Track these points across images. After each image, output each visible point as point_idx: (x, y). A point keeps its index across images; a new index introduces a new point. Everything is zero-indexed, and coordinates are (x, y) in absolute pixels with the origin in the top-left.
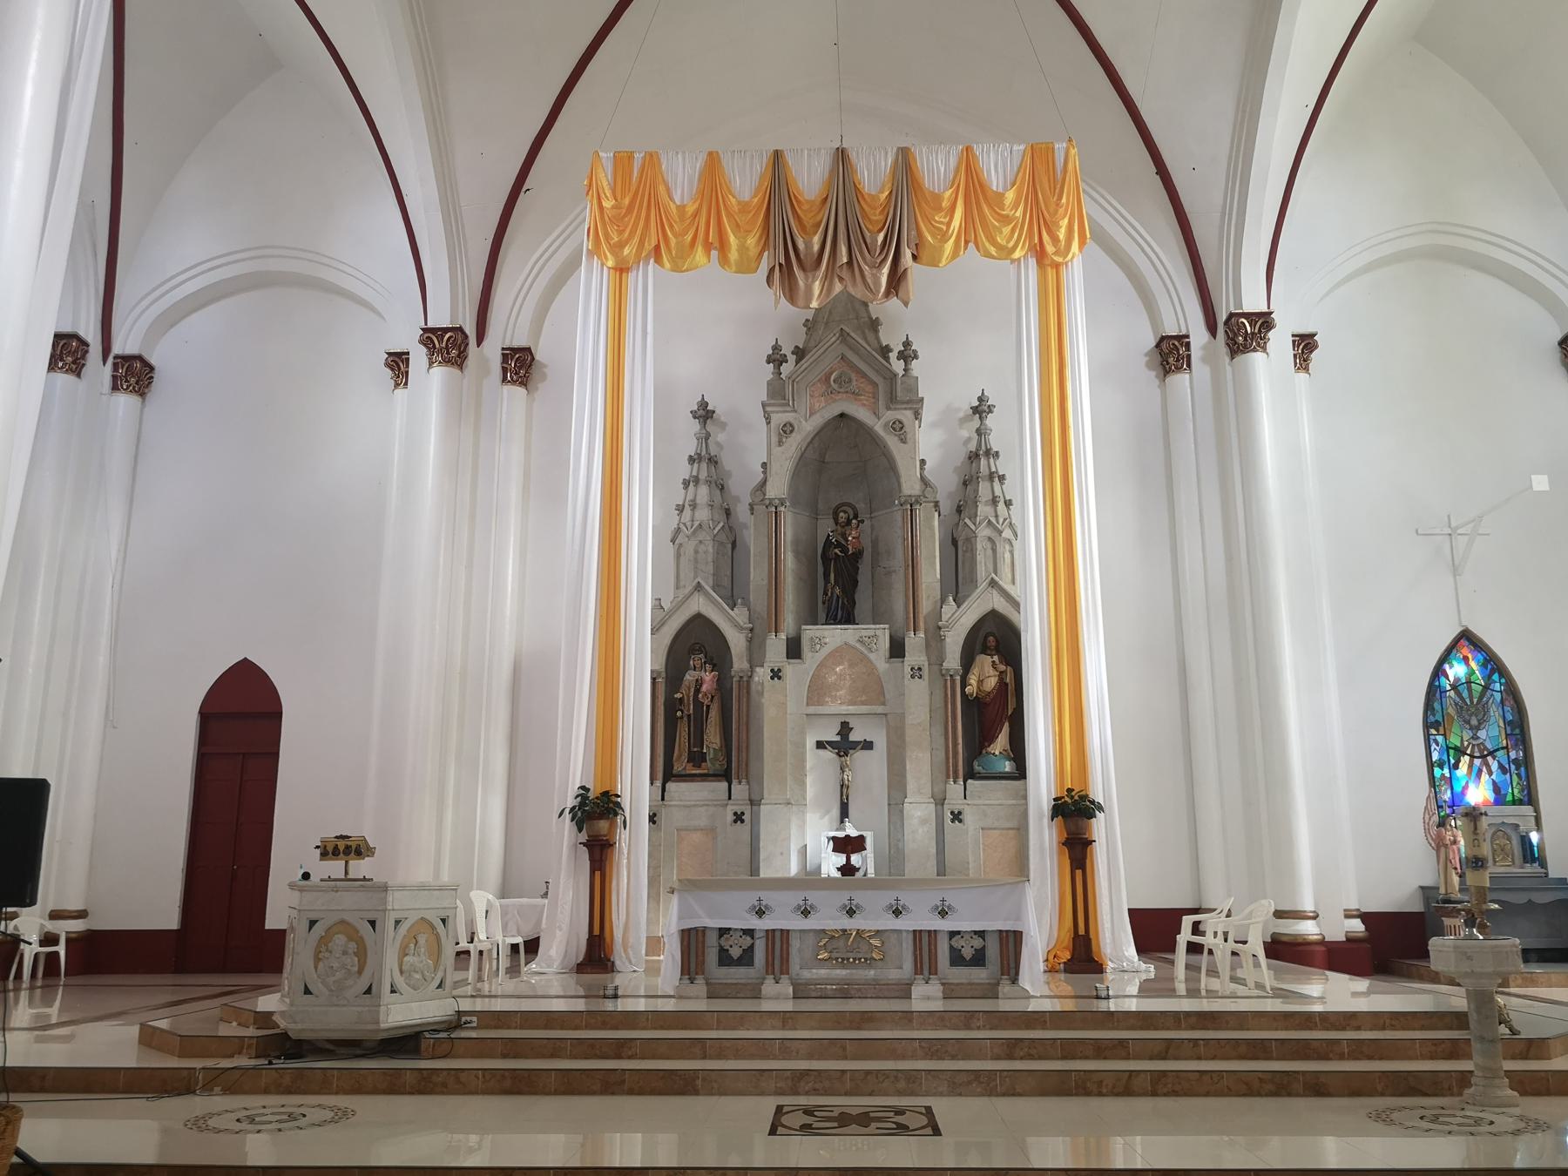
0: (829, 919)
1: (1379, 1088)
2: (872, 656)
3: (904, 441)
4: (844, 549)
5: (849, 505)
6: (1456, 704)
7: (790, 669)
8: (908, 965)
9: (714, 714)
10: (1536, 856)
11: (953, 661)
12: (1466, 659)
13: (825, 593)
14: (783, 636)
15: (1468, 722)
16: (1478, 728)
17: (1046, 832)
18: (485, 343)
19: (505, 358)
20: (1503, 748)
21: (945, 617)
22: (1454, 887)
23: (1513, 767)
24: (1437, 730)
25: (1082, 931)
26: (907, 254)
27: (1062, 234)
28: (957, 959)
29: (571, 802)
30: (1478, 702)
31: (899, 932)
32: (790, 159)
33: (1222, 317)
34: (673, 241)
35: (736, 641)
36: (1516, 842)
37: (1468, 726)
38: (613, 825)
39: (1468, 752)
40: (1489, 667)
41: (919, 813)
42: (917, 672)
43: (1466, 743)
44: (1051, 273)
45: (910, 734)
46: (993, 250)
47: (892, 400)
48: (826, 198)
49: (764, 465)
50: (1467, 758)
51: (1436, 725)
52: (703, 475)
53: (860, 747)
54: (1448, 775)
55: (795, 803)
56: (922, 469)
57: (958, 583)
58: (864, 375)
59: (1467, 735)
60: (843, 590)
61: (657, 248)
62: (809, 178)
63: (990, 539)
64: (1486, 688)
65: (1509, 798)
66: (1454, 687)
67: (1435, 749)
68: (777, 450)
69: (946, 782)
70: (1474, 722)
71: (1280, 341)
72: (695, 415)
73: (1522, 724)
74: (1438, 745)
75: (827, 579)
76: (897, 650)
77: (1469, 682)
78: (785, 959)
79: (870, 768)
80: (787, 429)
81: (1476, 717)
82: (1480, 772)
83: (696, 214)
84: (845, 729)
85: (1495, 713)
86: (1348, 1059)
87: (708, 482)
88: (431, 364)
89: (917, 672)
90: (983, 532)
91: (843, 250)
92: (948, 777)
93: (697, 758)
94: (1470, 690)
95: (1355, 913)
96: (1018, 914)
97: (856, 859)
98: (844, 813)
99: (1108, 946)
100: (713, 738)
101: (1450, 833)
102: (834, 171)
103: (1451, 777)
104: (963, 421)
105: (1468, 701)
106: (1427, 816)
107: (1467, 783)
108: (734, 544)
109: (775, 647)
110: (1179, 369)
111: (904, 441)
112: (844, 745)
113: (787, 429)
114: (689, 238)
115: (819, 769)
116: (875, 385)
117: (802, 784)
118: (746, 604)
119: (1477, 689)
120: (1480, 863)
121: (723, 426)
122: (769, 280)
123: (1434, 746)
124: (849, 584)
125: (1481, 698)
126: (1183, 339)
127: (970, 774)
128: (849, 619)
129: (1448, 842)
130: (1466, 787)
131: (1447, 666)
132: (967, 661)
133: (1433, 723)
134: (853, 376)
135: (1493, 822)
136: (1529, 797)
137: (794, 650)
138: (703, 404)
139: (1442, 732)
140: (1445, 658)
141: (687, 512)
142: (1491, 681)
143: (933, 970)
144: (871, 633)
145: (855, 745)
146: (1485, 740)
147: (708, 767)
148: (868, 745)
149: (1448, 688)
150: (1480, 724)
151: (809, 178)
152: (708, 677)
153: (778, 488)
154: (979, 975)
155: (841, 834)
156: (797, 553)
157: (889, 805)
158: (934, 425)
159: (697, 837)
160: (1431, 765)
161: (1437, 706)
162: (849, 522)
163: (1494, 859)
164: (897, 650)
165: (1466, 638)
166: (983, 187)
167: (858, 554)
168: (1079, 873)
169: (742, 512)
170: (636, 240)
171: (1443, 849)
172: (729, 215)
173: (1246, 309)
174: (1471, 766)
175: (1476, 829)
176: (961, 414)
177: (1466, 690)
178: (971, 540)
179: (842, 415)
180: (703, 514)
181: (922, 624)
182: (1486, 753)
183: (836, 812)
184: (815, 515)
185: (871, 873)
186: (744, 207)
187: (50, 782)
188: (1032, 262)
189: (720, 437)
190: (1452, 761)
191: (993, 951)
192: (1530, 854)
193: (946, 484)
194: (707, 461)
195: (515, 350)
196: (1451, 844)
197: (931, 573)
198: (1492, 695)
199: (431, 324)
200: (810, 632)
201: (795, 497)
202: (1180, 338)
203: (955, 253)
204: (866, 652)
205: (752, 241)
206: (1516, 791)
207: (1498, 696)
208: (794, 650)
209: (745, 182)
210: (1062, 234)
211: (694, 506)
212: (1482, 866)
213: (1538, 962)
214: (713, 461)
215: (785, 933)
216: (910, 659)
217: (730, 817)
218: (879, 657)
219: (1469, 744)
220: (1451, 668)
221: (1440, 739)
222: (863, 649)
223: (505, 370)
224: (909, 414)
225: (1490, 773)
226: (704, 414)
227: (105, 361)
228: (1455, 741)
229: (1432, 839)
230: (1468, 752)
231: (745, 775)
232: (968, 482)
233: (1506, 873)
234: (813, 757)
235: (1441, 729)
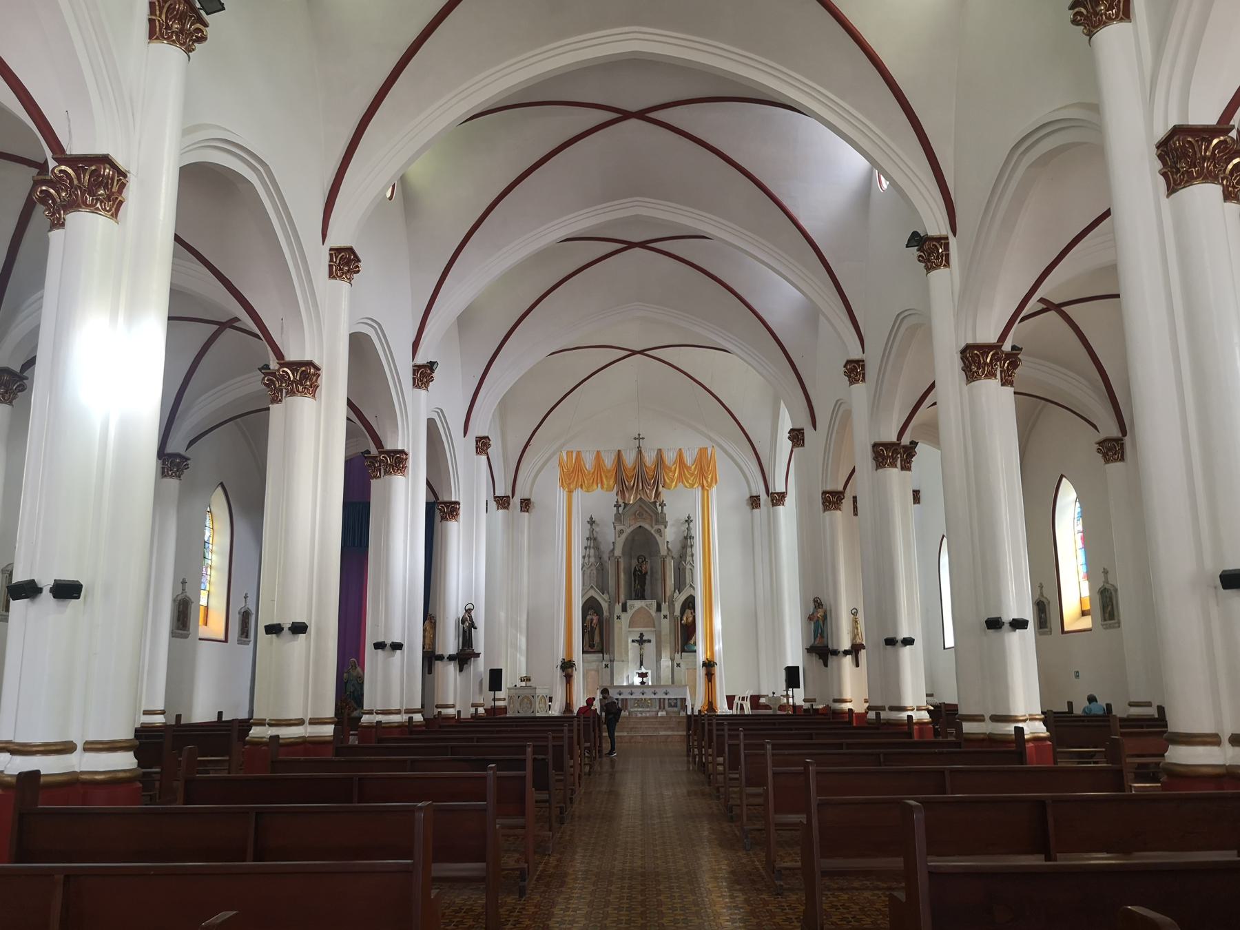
0: (637, 695)
3: (661, 536)
4: (641, 572)
5: (642, 556)
7: (623, 616)
8: (658, 708)
9: (597, 631)
11: (677, 612)
13: (635, 587)
14: (621, 604)
17: (701, 670)
18: (514, 497)
19: (521, 503)
21: (675, 597)
26: (660, 486)
27: (709, 480)
28: (670, 705)
29: (560, 664)
31: (655, 699)
32: (623, 453)
34: (586, 482)
35: (605, 606)
38: (572, 671)
41: (666, 662)
42: (665, 617)
44: (705, 492)
45: (663, 639)
46: (687, 485)
47: (657, 522)
48: (635, 468)
49: (613, 543)
52: (592, 545)
55: (624, 661)
56: (667, 545)
57: (680, 585)
58: (647, 512)
60: (641, 586)
61: (582, 485)
62: (629, 459)
63: (691, 569)
68: (618, 539)
69: (675, 653)
72: (588, 522)
75: (635, 581)
76: (659, 609)
78: (626, 706)
79: (650, 649)
80: (621, 532)
83: (594, 472)
84: (642, 635)
87: (593, 548)
88: (498, 509)
89: (665, 617)
90: (688, 567)
91: (641, 485)
93: (592, 646)
96: (685, 694)
97: (645, 679)
98: (641, 664)
100: (597, 638)
102: (637, 457)
104: (683, 523)
108: (603, 570)
109: (618, 608)
110: (757, 508)
111: (661, 536)
112: (641, 641)
113: (621, 532)
114: (591, 481)
115: (633, 649)
116: (651, 516)
117: (627, 653)
118: (608, 593)
121: (598, 525)
122: (617, 494)
124: (643, 584)
126: (758, 497)
127: (683, 651)
128: (643, 597)
132: (682, 613)
134: (644, 513)
137: (624, 609)
138: (591, 518)
141: (587, 558)
143: (664, 708)
145: (645, 641)
147: (596, 648)
148: (649, 641)
151: (629, 459)
152: (595, 618)
153: (618, 552)
154: (676, 709)
155: (640, 672)
156: (625, 574)
158: (673, 525)
159: (593, 672)
162: (643, 562)
164: (659, 609)
166: (685, 465)
167: (646, 573)
168: (710, 683)
169: (606, 557)
170: (575, 482)
172: (604, 472)
173: (777, 491)
176: (681, 521)
178: (684, 569)
179: (640, 527)
180: (592, 560)
181: (667, 600)
183: (639, 664)
184: (631, 558)
185: (650, 684)
186: (609, 471)
188: (700, 488)
189: (597, 529)
191: (679, 703)
193: (676, 549)
194: (593, 541)
195: (525, 500)
197: (670, 582)
199: (496, 495)
200: (629, 603)
201: (624, 553)
202: (756, 497)
203: (676, 486)
205: (612, 482)
208: (624, 609)
209: (609, 462)
210: (709, 480)
211: (589, 557)
214: (595, 539)
215: (626, 699)
217: (604, 666)
218: (653, 612)
223: (521, 507)
224: (663, 527)
231: (608, 652)
232: (684, 547)
234: (630, 645)
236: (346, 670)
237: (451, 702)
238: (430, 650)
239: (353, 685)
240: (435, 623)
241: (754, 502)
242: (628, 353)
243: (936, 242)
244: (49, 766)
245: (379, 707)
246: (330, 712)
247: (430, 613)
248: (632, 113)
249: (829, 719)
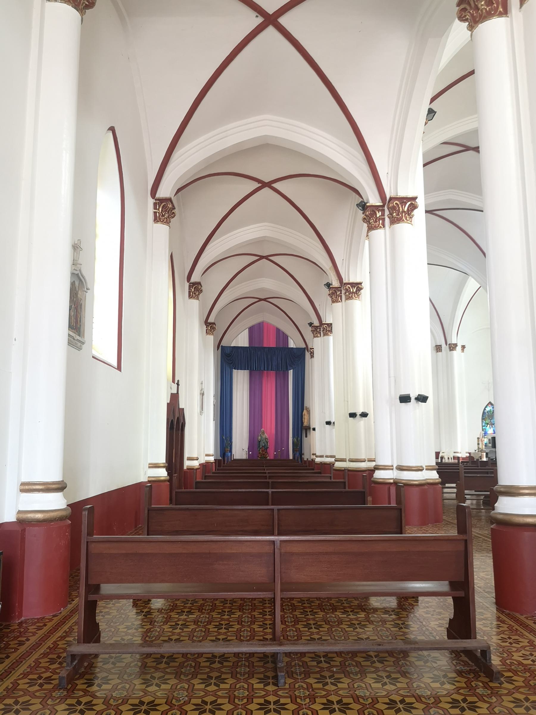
16: (491, 420)
33: (448, 343)
51: (484, 419)
59: (489, 421)
66: (487, 412)
71: (459, 348)
94: (490, 413)
110: (440, 351)
131: (486, 408)
133: (483, 419)
140: (486, 407)
160: (483, 426)
161: (484, 415)
165: (490, 403)
173: (453, 343)
187: (470, 711)
226: (364, 415)
227: (178, 381)
228: (487, 422)
236: (260, 435)
237: (195, 455)
238: (307, 425)
239: (264, 443)
240: (309, 411)
241: (438, 348)
242: (257, 258)
243: (398, 201)
244: (407, 476)
245: (329, 454)
246: (162, 459)
247: (305, 406)
248: (471, 147)
249: (302, 464)
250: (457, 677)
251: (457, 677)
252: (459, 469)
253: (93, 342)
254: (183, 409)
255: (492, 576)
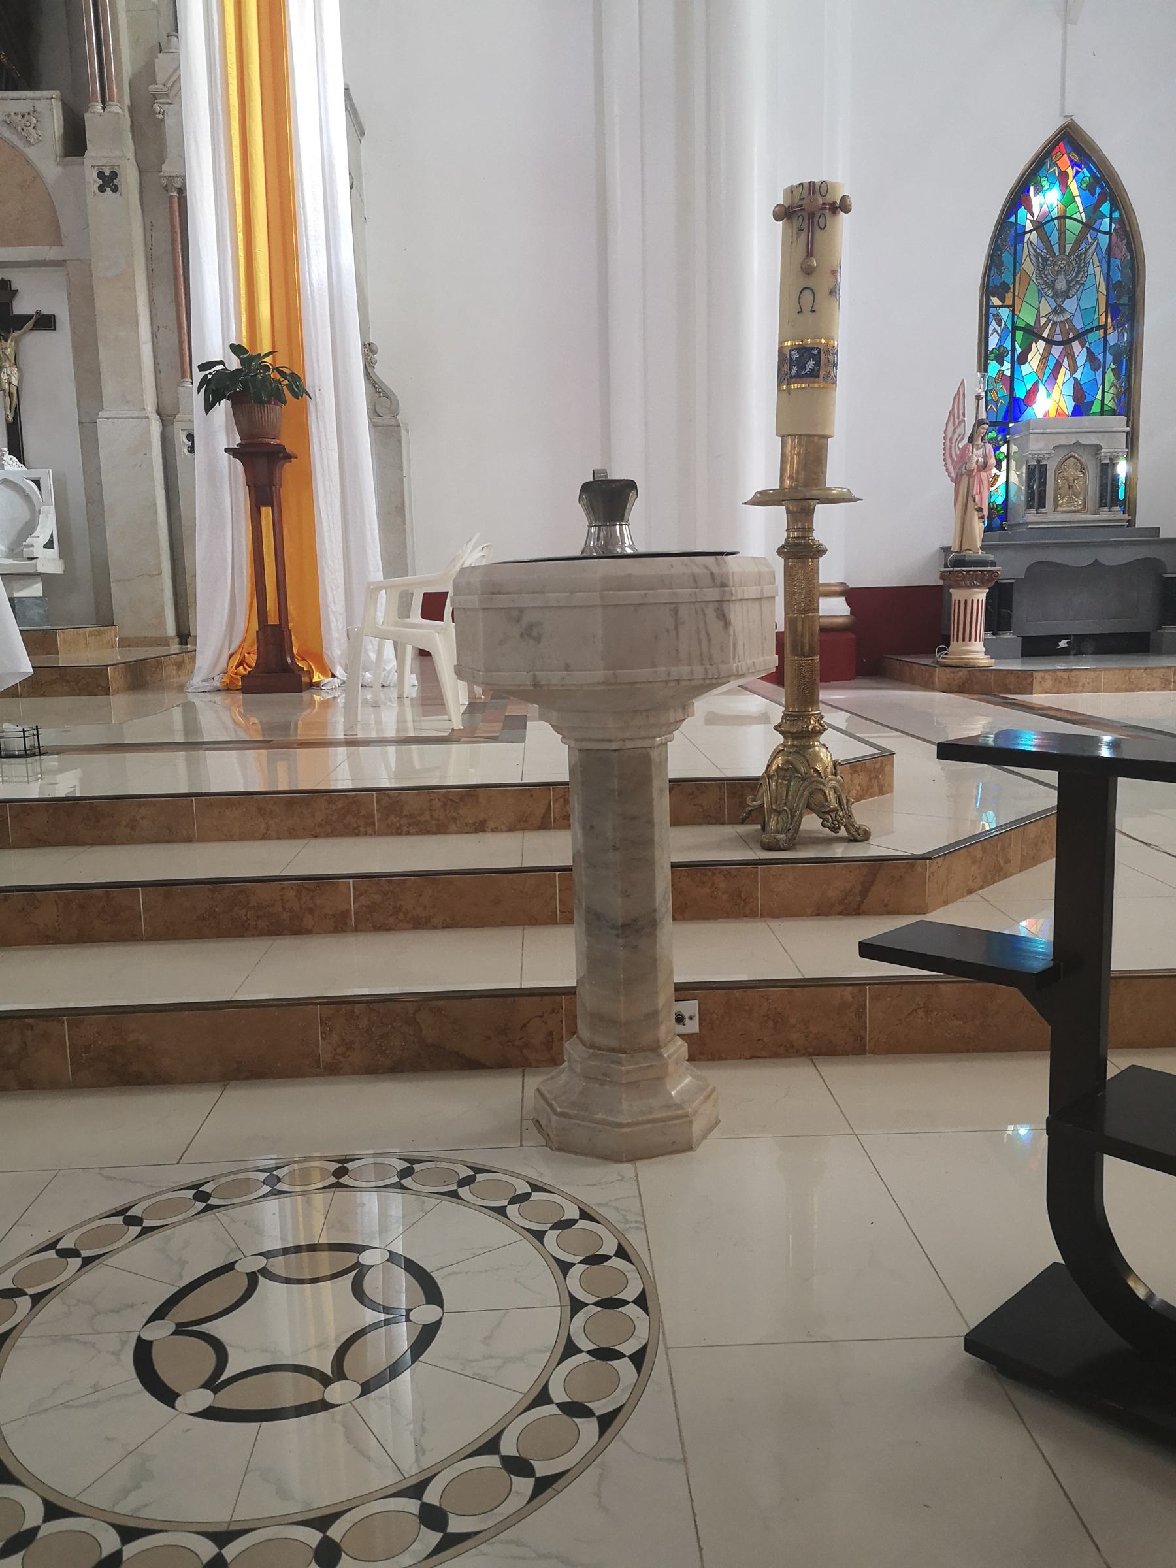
1: (324, 1053)
2: (31, 152)
6: (1037, 255)
10: (1121, 496)
12: (1063, 178)
15: (1052, 285)
20: (1098, 328)
22: (973, 540)
23: (1109, 358)
24: (1003, 300)
25: (273, 619)
30: (1072, 252)
36: (1092, 473)
37: (1050, 292)
39: (1045, 335)
40: (1098, 190)
43: (1043, 321)
50: (1041, 344)
53: (30, 324)
54: (1008, 373)
64: (1088, 226)
65: (1096, 408)
66: (1039, 226)
67: (995, 330)
70: (1061, 285)
73: (1134, 287)
74: (1000, 325)
77: (1063, 217)
81: (1066, 276)
82: (1058, 366)
85: (1095, 269)
86: (356, 930)
92: (183, 376)
94: (1062, 231)
95: (837, 589)
99: (335, 644)
101: (980, 452)
103: (1012, 378)
105: (1056, 248)
106: (951, 427)
107: (1036, 384)
119: (1073, 227)
120: (811, 364)
123: (993, 325)
125: (1077, 243)
129: (974, 466)
130: (1032, 393)
135: (1063, 443)
136: (1127, 405)
139: (1009, 302)
142: (1097, 214)
144: (24, 107)
146: (1073, 315)
148: (46, 322)
149: (1029, 227)
150: (1069, 288)
157: (80, 423)
161: (1007, 258)
163: (1056, 500)
171: (965, 479)
174: (1045, 358)
175: (810, 252)
177: (1055, 232)
182: (1071, 335)
190: (1018, 350)
192: (1108, 492)
196: (979, 470)
198: (1095, 239)
204: (20, 144)
206: (1108, 397)
207: (1104, 240)
212: (814, 374)
213: (1094, 653)
216: (93, 154)
219: (1049, 320)
220: (1037, 192)
221: (1005, 313)
222: (14, 139)
225: (1073, 369)
228: (1027, 316)
229: (952, 460)
230: (1045, 335)
233: (1070, 522)
235: (1009, 296)
250: (628, 1271)
251: (628, 1271)
252: (964, 640)
253: (1046, 1114)
254: (411, 673)
255: (378, 570)
